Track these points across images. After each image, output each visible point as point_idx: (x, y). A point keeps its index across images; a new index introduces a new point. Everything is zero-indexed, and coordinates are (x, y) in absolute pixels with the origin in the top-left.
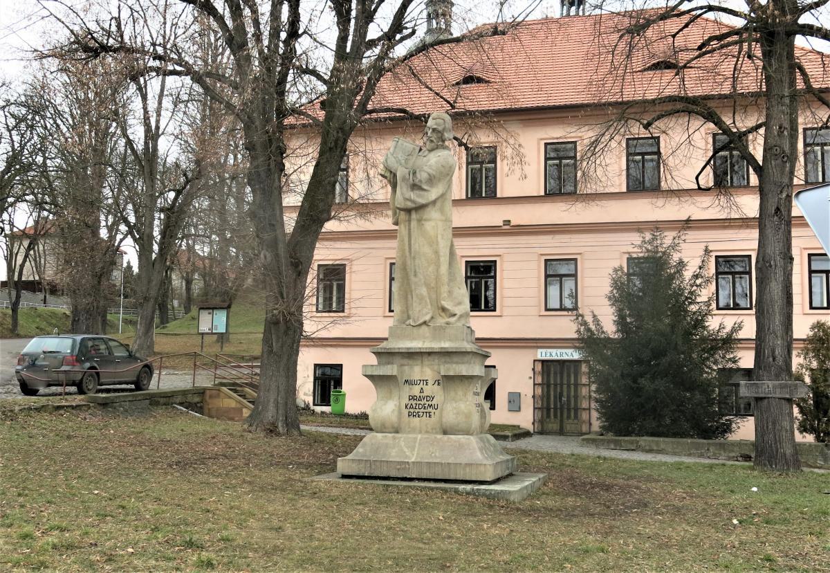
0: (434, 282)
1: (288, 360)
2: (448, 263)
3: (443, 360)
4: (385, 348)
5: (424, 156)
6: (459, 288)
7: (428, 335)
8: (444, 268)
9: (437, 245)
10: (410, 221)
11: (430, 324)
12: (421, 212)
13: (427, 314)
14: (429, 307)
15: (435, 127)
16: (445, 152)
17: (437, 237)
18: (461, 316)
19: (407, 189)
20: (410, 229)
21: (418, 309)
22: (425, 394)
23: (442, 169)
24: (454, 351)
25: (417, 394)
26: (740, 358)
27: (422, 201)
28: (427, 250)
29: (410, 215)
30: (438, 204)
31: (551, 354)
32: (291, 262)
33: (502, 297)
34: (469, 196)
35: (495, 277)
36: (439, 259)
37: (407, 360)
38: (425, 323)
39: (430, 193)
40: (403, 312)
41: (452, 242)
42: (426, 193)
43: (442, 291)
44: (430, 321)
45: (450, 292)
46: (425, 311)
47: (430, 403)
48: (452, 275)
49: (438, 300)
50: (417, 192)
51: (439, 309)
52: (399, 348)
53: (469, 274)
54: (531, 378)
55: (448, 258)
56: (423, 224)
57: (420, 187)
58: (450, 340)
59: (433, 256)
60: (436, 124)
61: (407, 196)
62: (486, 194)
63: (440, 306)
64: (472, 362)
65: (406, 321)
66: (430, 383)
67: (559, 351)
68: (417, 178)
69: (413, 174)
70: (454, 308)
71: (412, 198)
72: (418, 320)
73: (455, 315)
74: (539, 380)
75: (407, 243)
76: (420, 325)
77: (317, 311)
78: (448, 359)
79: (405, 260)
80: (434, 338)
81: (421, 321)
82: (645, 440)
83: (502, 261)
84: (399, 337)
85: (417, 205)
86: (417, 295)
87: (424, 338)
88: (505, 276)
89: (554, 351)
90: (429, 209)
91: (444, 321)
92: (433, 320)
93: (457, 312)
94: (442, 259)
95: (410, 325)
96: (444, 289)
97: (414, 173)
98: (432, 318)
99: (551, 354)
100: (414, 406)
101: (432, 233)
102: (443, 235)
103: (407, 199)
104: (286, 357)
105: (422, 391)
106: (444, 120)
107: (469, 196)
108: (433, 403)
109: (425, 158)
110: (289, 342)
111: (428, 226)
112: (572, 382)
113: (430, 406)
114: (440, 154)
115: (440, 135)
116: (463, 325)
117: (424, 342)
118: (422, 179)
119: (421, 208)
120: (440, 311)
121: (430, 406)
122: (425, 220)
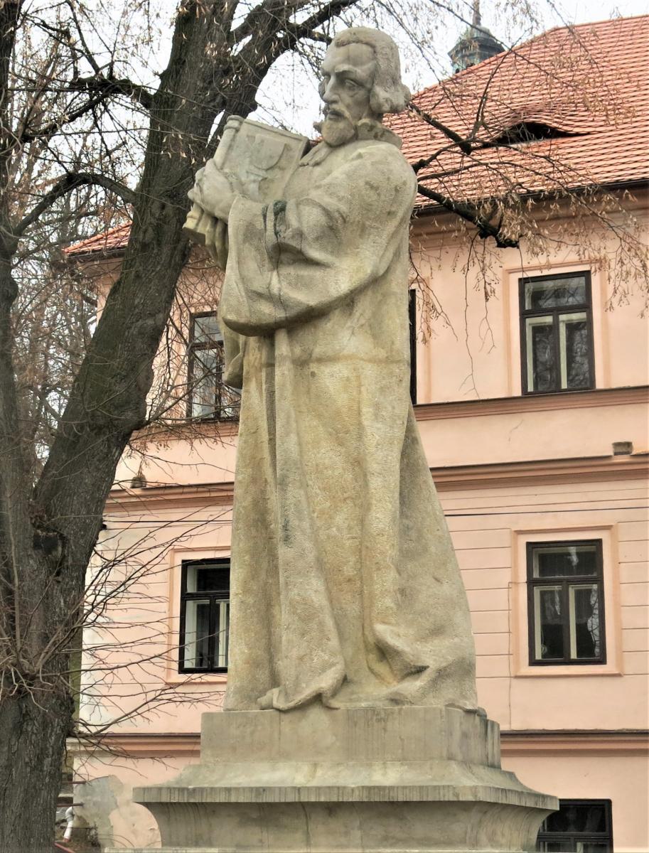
0: (353, 559)
1: (25, 804)
2: (397, 495)
3: (378, 831)
4: (182, 790)
5: (317, 164)
6: (438, 580)
7: (330, 739)
8: (383, 514)
9: (360, 437)
10: (271, 365)
11: (334, 703)
12: (306, 336)
13: (325, 667)
14: (334, 642)
15: (345, 67)
16: (382, 147)
17: (359, 413)
18: (442, 674)
19: (261, 266)
20: (271, 394)
21: (295, 653)
23: (372, 196)
24: (416, 798)
27: (306, 298)
28: (327, 456)
29: (272, 346)
30: (364, 307)
32: (37, 536)
33: (620, 629)
34: (530, 388)
35: (600, 581)
36: (366, 485)
37: (257, 830)
38: (318, 699)
39: (331, 272)
40: (254, 664)
41: (410, 430)
42: (317, 273)
43: (377, 588)
44: (335, 692)
45: (405, 594)
46: (319, 657)
48: (413, 534)
49: (364, 621)
50: (291, 271)
51: (368, 651)
52: (228, 790)
53: (536, 575)
55: (394, 479)
56: (313, 374)
57: (300, 252)
58: (403, 760)
59: (349, 476)
60: (348, 59)
61: (258, 285)
62: (570, 381)
63: (371, 640)
64: (483, 838)
65: (263, 692)
68: (288, 226)
69: (276, 214)
70: (419, 646)
71: (275, 291)
72: (296, 691)
73: (420, 670)
75: (265, 436)
76: (302, 707)
77: (182, 670)
78: (395, 829)
79: (263, 492)
80: (351, 752)
81: (307, 692)
83: (615, 542)
84: (234, 749)
85: (292, 313)
86: (292, 604)
87: (313, 752)
88: (624, 577)
90: (328, 325)
91: (385, 691)
92: (347, 690)
93: (432, 663)
94: (375, 483)
95: (270, 707)
96: (386, 581)
97: (280, 210)
98: (345, 680)
101: (342, 400)
102: (377, 407)
103: (260, 295)
104: (18, 795)
106: (373, 47)
107: (530, 388)
109: (318, 169)
110: (28, 754)
111: (331, 378)
114: (361, 151)
115: (361, 93)
116: (451, 705)
117: (315, 765)
118: (305, 230)
119: (306, 319)
120: (373, 657)
122: (320, 360)
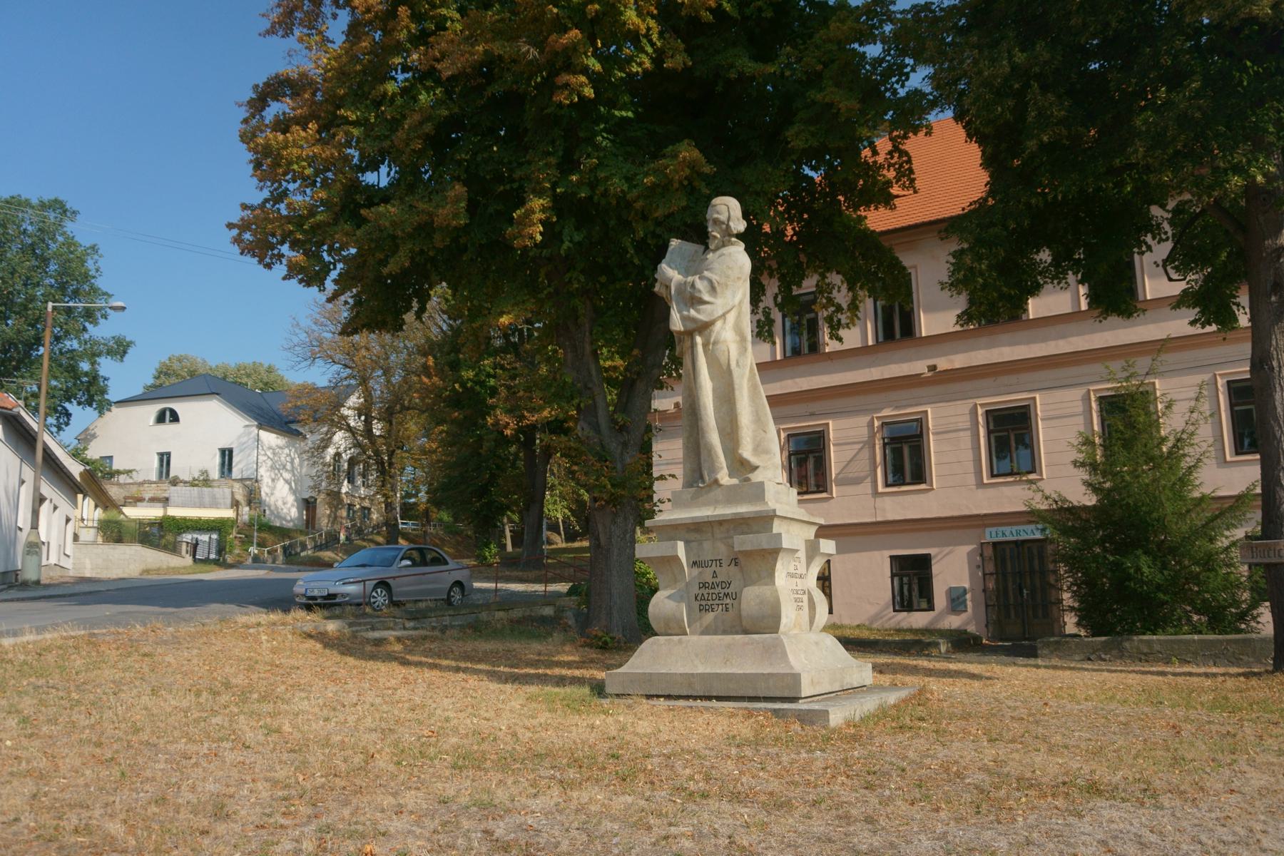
22: (718, 580)
25: (710, 580)
26: (660, 511)
31: (1003, 534)
47: (726, 591)
53: (1233, 401)
54: (978, 567)
66: (725, 564)
67: (1014, 529)
74: (990, 568)
82: (1148, 642)
89: (1007, 530)
99: (1003, 534)
100: (706, 596)
105: (715, 575)
108: (730, 591)
112: (1037, 567)
113: (727, 595)
121: (727, 595)
